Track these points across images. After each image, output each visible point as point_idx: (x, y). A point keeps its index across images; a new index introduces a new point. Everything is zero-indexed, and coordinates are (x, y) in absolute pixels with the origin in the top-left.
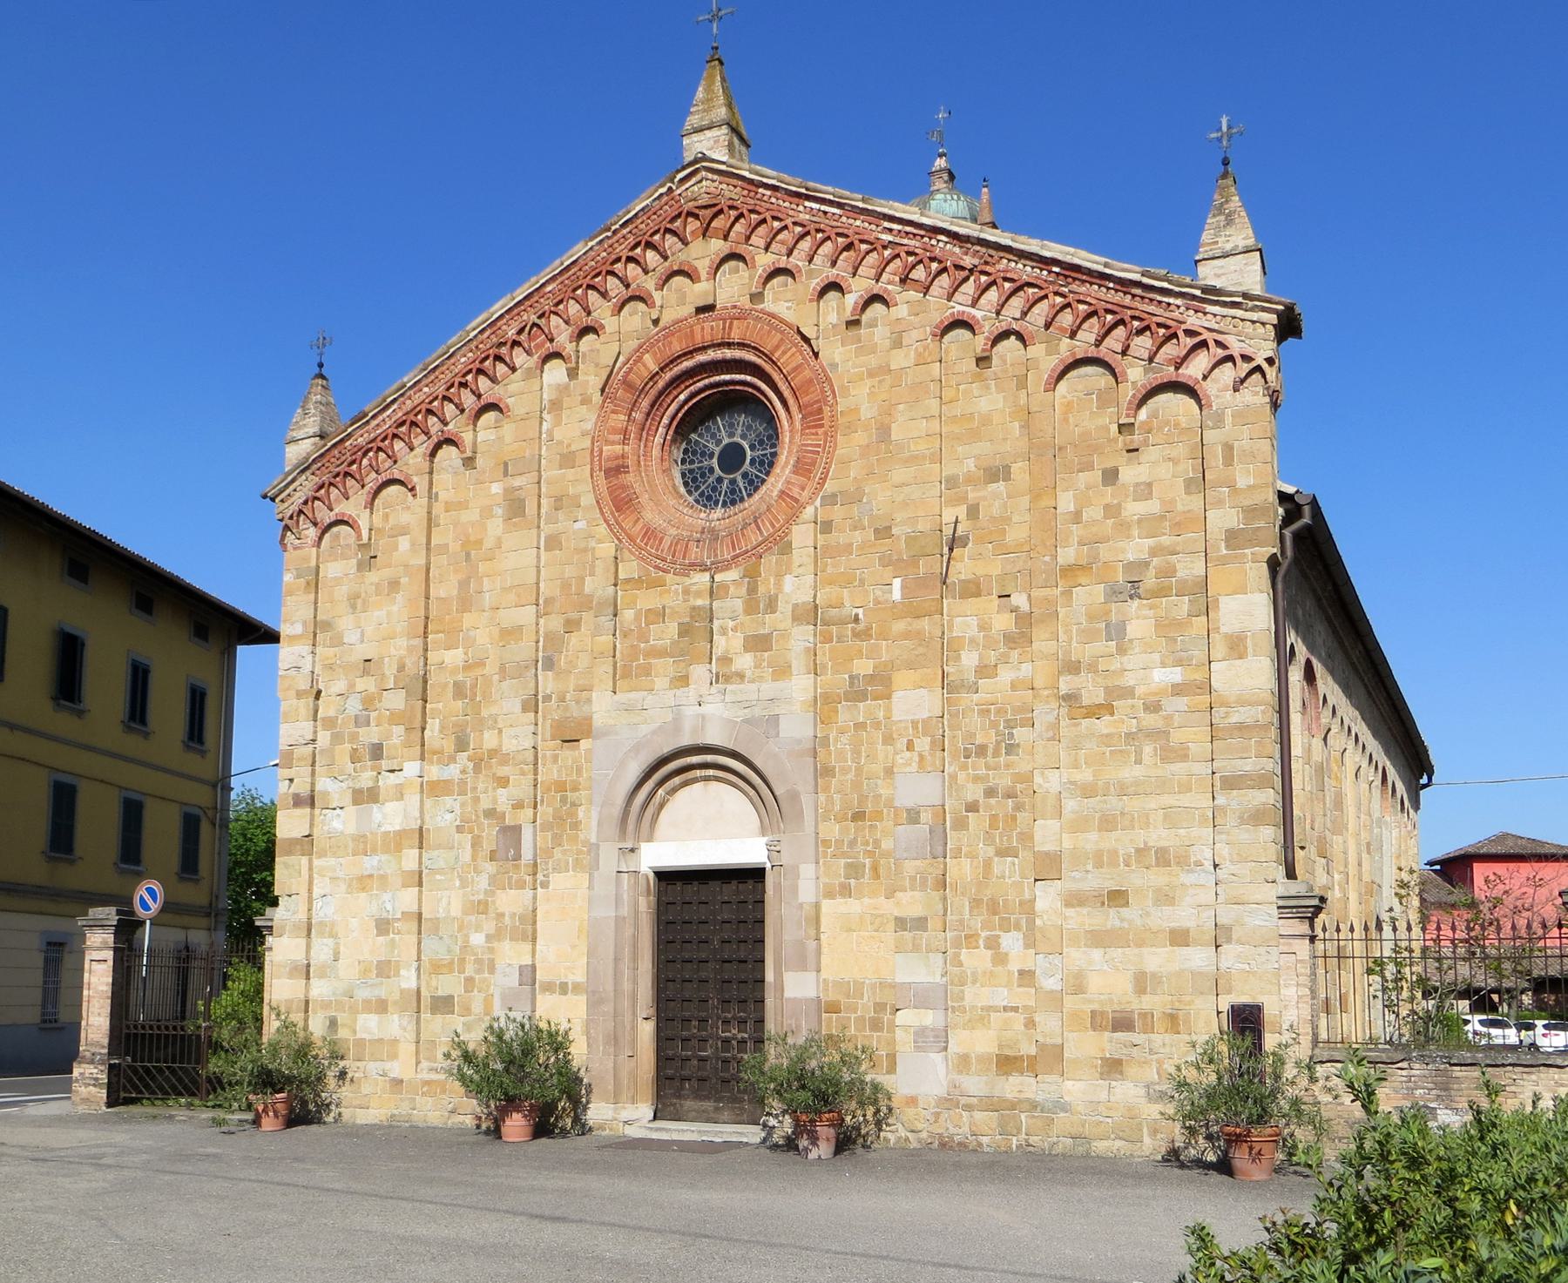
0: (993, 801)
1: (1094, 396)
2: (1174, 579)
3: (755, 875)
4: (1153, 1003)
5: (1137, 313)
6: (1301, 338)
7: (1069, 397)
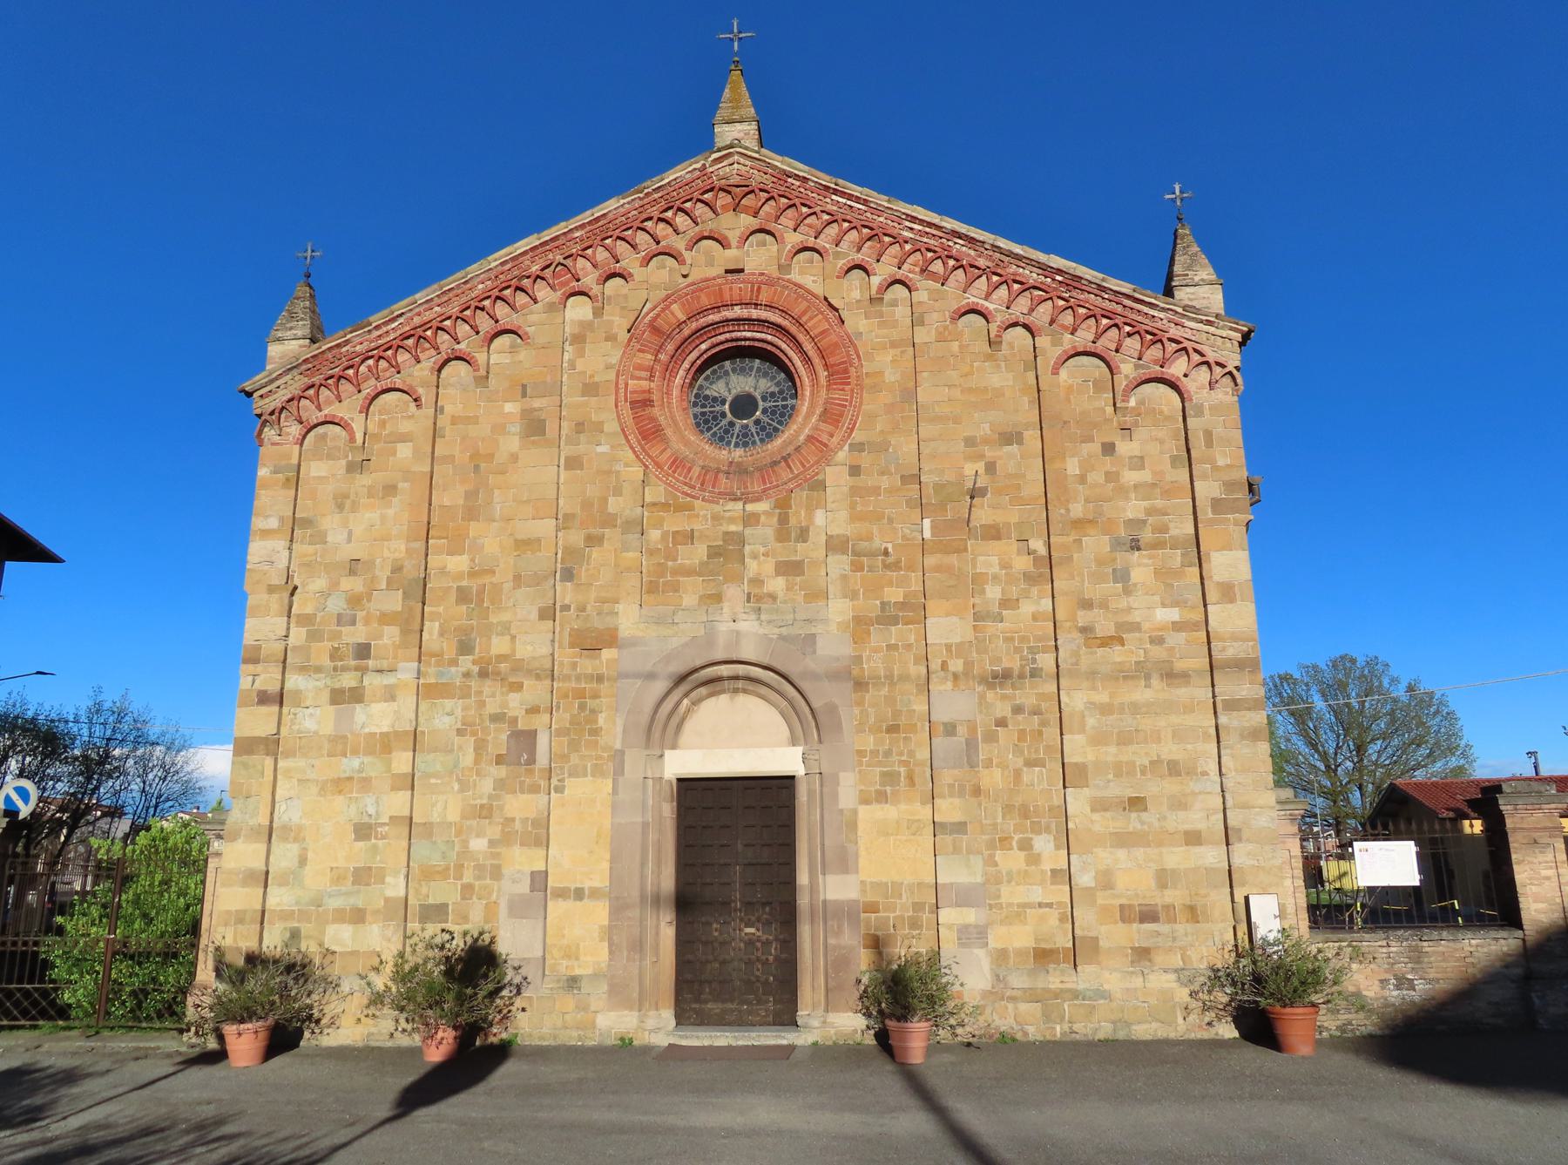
4: (1174, 896)
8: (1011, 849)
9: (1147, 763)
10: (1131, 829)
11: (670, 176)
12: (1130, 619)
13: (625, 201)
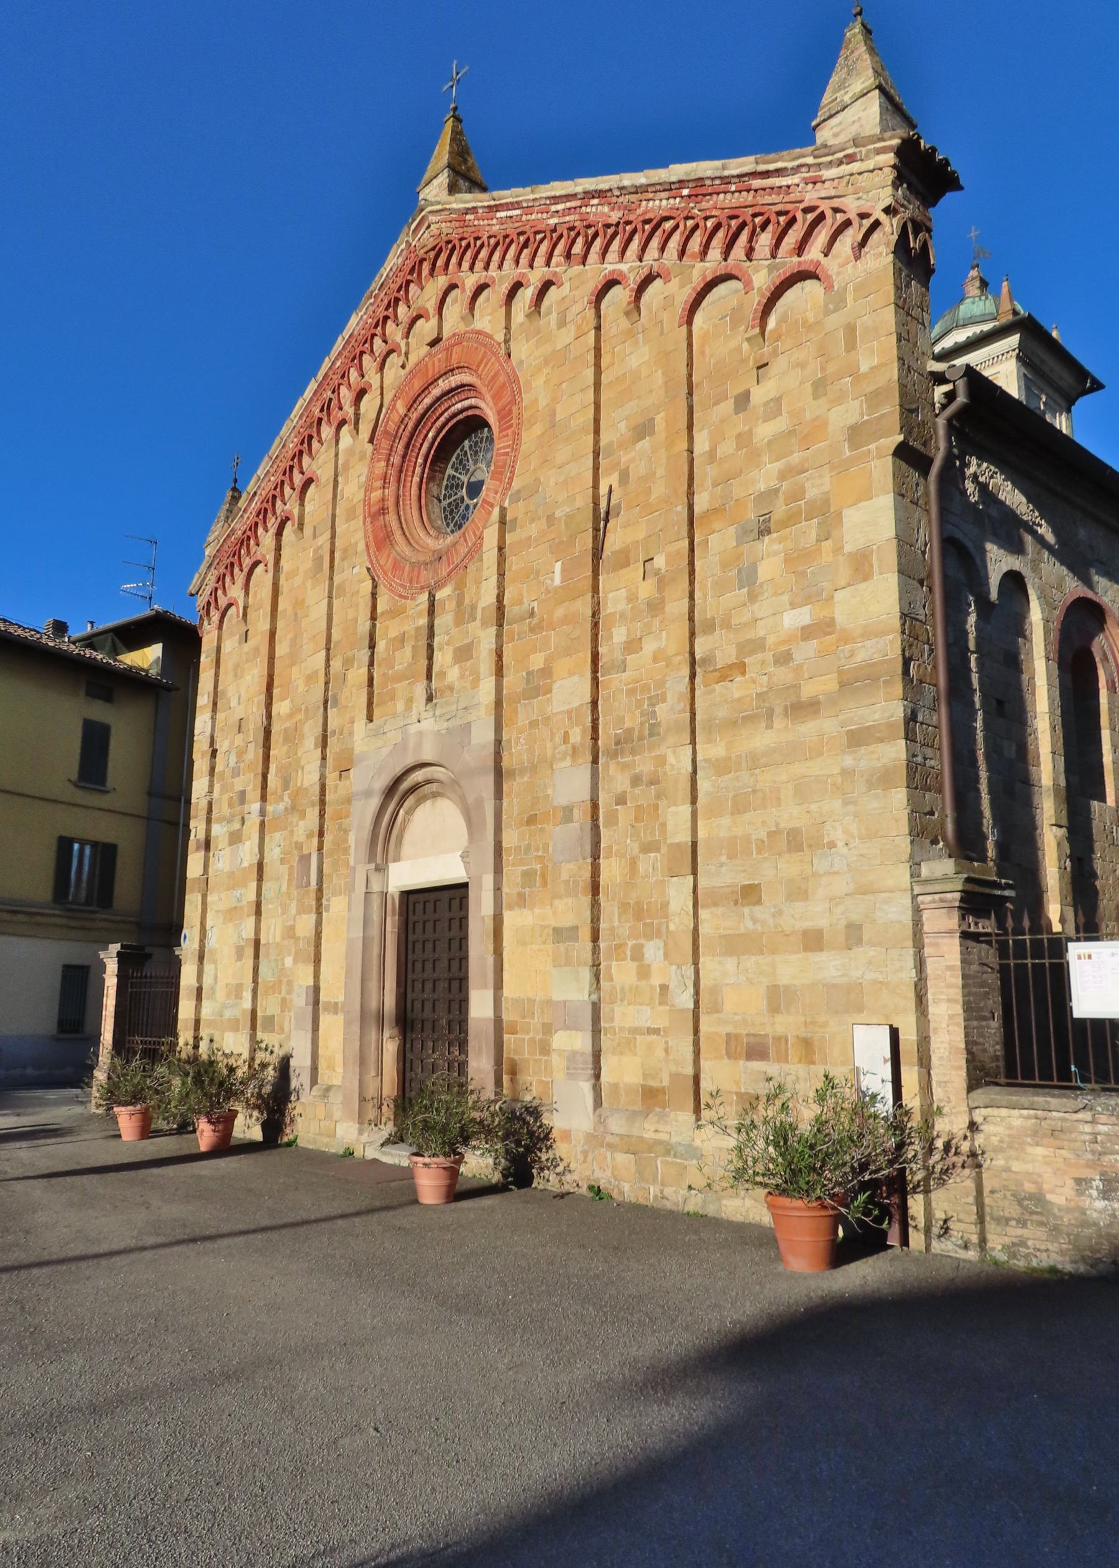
0: (637, 791)
1: (728, 318)
2: (803, 502)
3: (465, 885)
4: (786, 1024)
5: (757, 210)
6: (961, 188)
7: (705, 327)
8: (624, 959)
9: (763, 835)
10: (742, 930)
11: (385, 271)
12: (751, 635)
13: (362, 313)
